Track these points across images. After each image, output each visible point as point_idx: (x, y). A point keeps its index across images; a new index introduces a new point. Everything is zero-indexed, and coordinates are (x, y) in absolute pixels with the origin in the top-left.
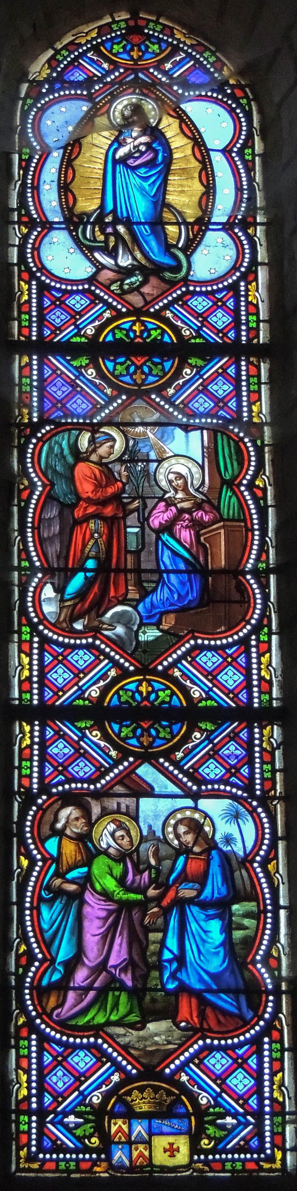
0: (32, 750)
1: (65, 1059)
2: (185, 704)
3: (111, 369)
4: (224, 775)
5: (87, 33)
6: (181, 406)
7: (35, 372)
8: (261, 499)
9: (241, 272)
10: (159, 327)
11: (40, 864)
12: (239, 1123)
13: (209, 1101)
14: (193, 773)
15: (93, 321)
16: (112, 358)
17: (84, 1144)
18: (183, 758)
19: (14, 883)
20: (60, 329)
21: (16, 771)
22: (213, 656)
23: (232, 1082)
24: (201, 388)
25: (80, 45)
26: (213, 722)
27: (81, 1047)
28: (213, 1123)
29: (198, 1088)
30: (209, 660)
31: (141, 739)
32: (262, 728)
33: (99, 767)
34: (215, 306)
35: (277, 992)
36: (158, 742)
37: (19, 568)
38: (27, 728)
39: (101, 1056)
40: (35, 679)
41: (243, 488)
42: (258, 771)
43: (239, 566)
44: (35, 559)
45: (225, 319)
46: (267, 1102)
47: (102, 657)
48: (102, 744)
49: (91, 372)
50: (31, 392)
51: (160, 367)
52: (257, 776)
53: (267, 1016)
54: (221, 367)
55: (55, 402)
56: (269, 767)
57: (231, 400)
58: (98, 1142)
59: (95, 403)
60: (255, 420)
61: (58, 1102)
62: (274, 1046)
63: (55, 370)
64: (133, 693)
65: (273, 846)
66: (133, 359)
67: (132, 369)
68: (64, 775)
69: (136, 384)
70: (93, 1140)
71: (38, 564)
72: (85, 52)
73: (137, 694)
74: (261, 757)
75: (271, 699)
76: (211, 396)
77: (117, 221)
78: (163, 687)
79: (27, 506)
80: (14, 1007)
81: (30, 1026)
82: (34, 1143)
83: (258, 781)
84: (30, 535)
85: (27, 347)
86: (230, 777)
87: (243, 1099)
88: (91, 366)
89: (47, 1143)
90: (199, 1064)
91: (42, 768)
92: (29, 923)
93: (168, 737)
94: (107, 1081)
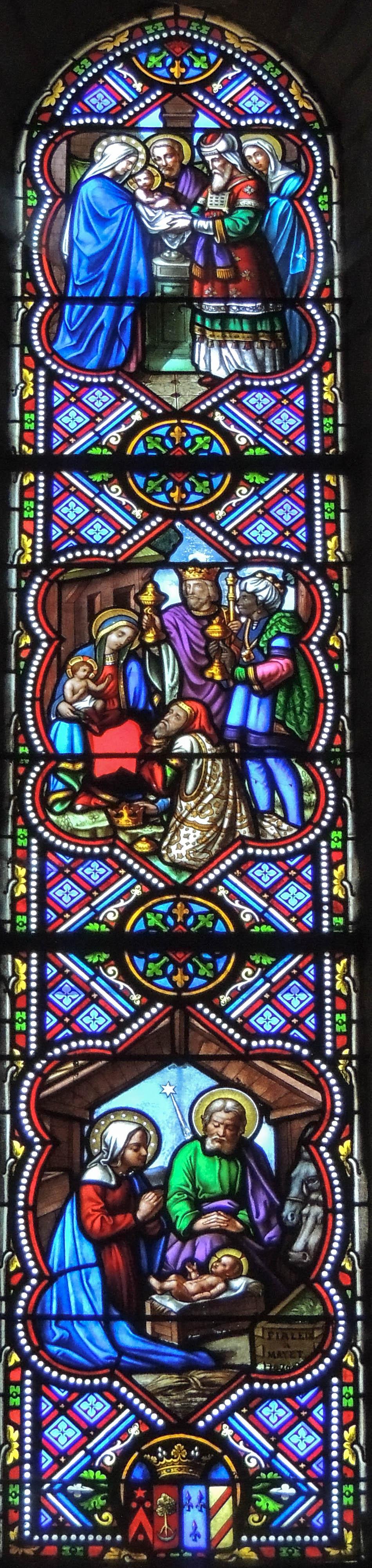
0: (29, 997)
1: (70, 1406)
2: (232, 929)
3: (141, 968)
5: (114, 37)
6: (230, 105)
8: (348, 1288)
9: (313, 362)
10: (207, 433)
14: (242, 1024)
15: (112, 1444)
19: (6, 1084)
22: (270, 868)
23: (290, 1439)
25: (106, 55)
26: (264, 474)
27: (92, 1390)
28: (265, 1492)
30: (266, 874)
32: (335, 961)
38: (22, 968)
39: (118, 1402)
40: (34, 898)
41: (322, 1149)
43: (298, 294)
44: (37, 742)
45: (292, 422)
46: (335, 1464)
51: (206, 483)
52: (328, 1030)
53: (334, 1352)
54: (286, 486)
56: (344, 1017)
59: (118, 529)
60: (331, 559)
63: (62, 969)
67: (170, 968)
68: (71, 1030)
70: (105, 1515)
71: (40, 749)
72: (111, 65)
74: (332, 1005)
79: (27, 670)
81: (25, 1363)
83: (329, 1037)
86: (291, 1030)
89: (46, 1519)
91: (41, 1020)
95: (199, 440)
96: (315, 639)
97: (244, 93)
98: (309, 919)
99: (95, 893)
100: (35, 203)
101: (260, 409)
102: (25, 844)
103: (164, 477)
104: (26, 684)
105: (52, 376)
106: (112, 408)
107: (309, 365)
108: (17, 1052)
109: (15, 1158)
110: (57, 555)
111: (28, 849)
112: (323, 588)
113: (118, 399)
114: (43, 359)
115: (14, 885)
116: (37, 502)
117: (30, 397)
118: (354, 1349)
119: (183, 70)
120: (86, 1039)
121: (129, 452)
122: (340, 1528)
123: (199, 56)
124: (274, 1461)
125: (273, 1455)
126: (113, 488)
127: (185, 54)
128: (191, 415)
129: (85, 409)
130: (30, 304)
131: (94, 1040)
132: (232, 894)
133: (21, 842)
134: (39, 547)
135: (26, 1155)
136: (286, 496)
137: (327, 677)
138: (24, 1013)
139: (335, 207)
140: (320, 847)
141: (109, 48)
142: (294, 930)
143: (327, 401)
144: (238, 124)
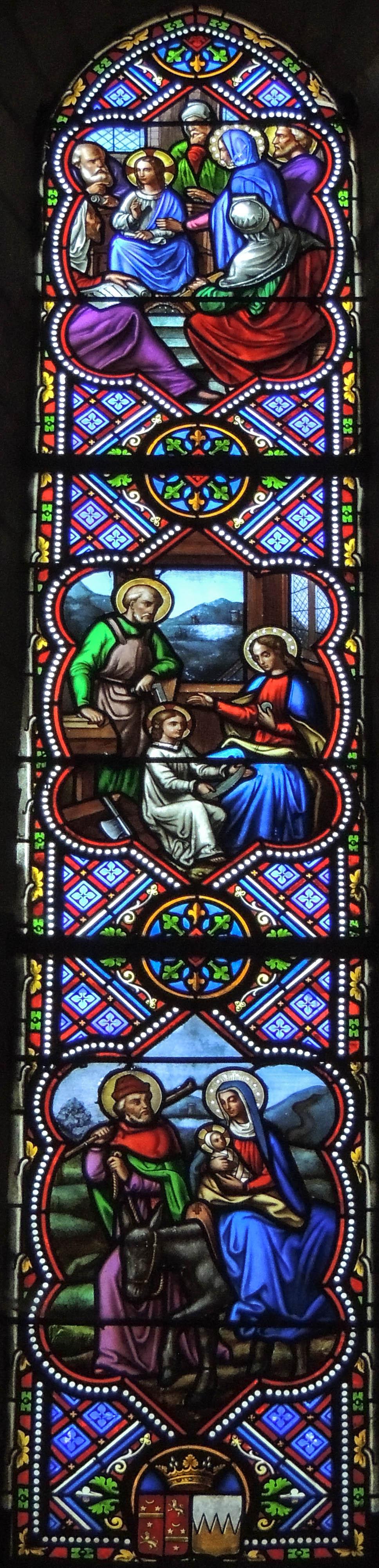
2: (249, 934)
6: (250, 98)
7: (39, 1425)
8: (360, 1294)
10: (227, 912)
11: (63, 650)
12: (308, 1497)
16: (163, 476)
17: (102, 1524)
19: (21, 1083)
20: (87, 915)
25: (126, 53)
26: (285, 959)
29: (254, 1454)
30: (279, 875)
31: (192, 64)
34: (298, 409)
35: (361, 1326)
36: (212, 985)
42: (341, 1029)
47: (144, 402)
55: (86, 437)
57: (323, 973)
58: (121, 1523)
60: (348, 563)
61: (80, 923)
63: (86, 490)
64: (181, 917)
65: (358, 1128)
66: (189, 478)
69: (191, 511)
70: (115, 1520)
71: (66, 293)
73: (185, 919)
76: (291, 529)
78: (221, 911)
81: (38, 1372)
82: (36, 1522)
84: (56, 257)
85: (51, 464)
88: (134, 486)
89: (54, 1524)
91: (56, 1020)
92: (36, 1192)
93: (226, 978)
95: (217, 919)
96: (331, 645)
97: (268, 527)
100: (55, 202)
101: (279, 412)
102: (29, 1409)
103: (181, 962)
104: (43, 689)
106: (131, 411)
107: (329, 367)
108: (32, 1052)
109: (29, 1158)
110: (67, 1047)
113: (139, 402)
115: (30, 982)
116: (55, 507)
117: (50, 400)
118: (364, 1355)
119: (203, 64)
121: (149, 453)
122: (351, 1529)
123: (218, 49)
125: (282, 913)
126: (132, 494)
127: (204, 49)
133: (40, 845)
136: (302, 501)
137: (344, 683)
139: (354, 202)
141: (129, 47)
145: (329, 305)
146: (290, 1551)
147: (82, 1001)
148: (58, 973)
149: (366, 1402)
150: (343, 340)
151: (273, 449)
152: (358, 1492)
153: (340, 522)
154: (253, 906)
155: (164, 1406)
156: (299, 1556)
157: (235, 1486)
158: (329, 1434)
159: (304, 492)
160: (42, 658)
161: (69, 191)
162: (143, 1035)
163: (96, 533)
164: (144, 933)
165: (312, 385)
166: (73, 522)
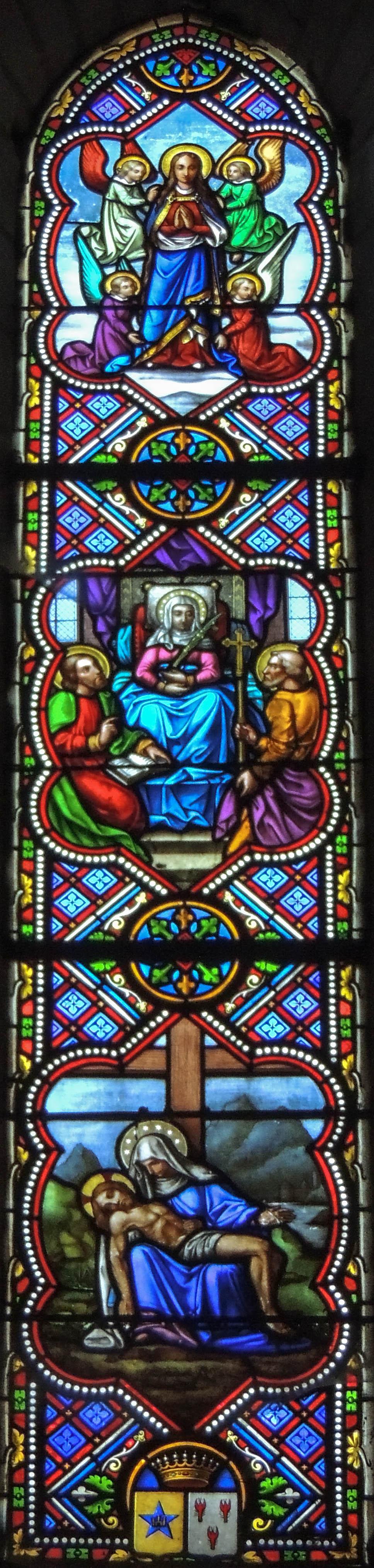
4: (287, 1034)
6: (244, 1029)
8: (339, 589)
10: (213, 915)
12: (303, 1497)
13: (264, 1468)
15: (123, 433)
18: (234, 1011)
20: (77, 920)
21: (16, 853)
24: (272, 1004)
26: (267, 481)
29: (250, 1451)
30: (270, 879)
33: (122, 1025)
35: (354, 1318)
37: (22, 768)
47: (129, 405)
48: (127, 992)
49: (118, 979)
50: (40, 440)
53: (339, 1355)
62: (349, 1394)
63: (71, 495)
70: (111, 1519)
75: (351, 929)
77: (154, 1180)
80: (19, 638)
81: (31, 1371)
86: (297, 1037)
87: (307, 1464)
89: (50, 1523)
90: (249, 1417)
94: (132, 426)
95: (204, 923)
98: (313, 924)
99: (97, 1440)
100: (42, 213)
105: (58, 384)
107: (316, 372)
111: (34, 860)
112: (326, 594)
113: (123, 405)
114: (41, 836)
117: (36, 407)
120: (92, 1048)
121: (133, 460)
124: (278, 1465)
125: (277, 1459)
128: (196, 422)
129: (89, 414)
130: (37, 313)
131: (100, 1048)
132: (239, 901)
134: (44, 557)
135: (31, 1162)
138: (23, 1392)
140: (317, 386)
141: (116, 57)
142: (300, 937)
143: (330, 491)
144: (246, 564)
145: (322, 769)
146: (286, 1553)
147: (72, 1005)
148: (48, 978)
149: (347, 761)
150: (328, 348)
151: (258, 455)
152: (352, 1493)
153: (325, 527)
154: (247, 1452)
155: (155, 1401)
156: (295, 1558)
157: (230, 1484)
158: (315, 893)
159: (289, 493)
160: (29, 667)
161: (48, 764)
162: (134, 1040)
163: (81, 537)
164: (132, 938)
165: (297, 390)
166: (58, 527)
